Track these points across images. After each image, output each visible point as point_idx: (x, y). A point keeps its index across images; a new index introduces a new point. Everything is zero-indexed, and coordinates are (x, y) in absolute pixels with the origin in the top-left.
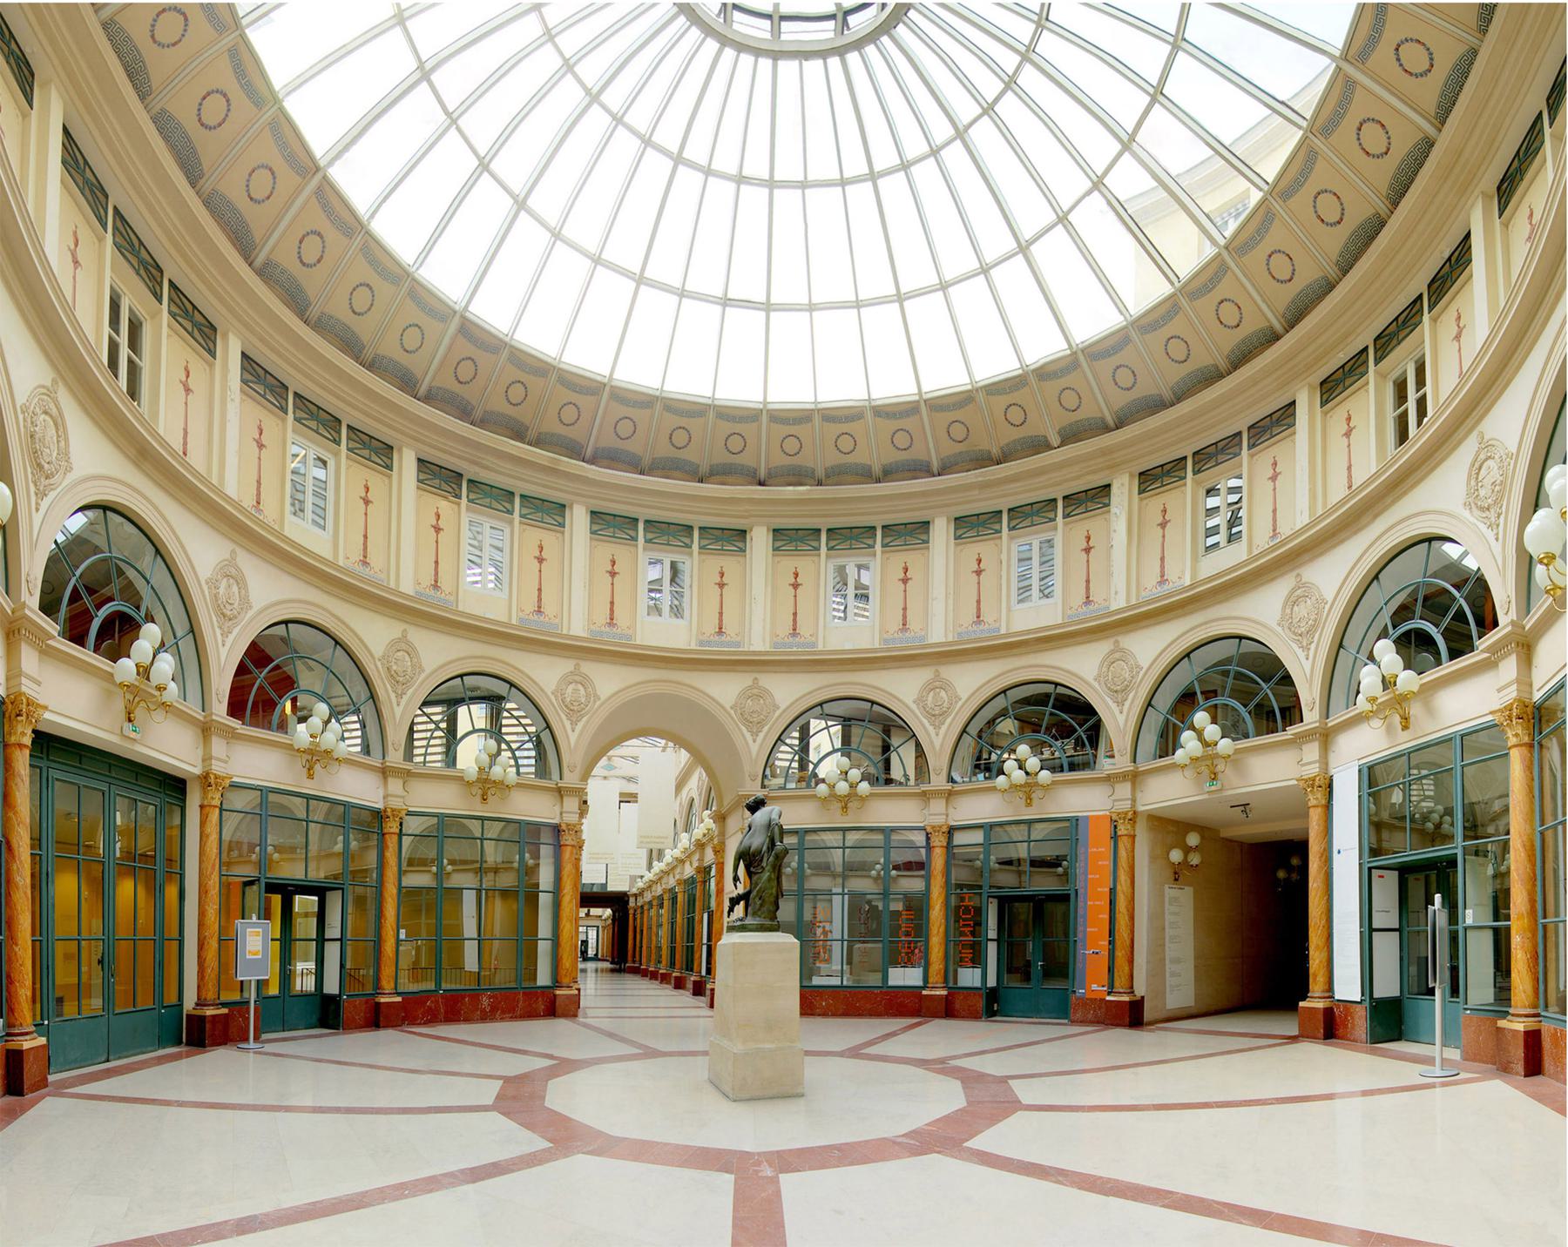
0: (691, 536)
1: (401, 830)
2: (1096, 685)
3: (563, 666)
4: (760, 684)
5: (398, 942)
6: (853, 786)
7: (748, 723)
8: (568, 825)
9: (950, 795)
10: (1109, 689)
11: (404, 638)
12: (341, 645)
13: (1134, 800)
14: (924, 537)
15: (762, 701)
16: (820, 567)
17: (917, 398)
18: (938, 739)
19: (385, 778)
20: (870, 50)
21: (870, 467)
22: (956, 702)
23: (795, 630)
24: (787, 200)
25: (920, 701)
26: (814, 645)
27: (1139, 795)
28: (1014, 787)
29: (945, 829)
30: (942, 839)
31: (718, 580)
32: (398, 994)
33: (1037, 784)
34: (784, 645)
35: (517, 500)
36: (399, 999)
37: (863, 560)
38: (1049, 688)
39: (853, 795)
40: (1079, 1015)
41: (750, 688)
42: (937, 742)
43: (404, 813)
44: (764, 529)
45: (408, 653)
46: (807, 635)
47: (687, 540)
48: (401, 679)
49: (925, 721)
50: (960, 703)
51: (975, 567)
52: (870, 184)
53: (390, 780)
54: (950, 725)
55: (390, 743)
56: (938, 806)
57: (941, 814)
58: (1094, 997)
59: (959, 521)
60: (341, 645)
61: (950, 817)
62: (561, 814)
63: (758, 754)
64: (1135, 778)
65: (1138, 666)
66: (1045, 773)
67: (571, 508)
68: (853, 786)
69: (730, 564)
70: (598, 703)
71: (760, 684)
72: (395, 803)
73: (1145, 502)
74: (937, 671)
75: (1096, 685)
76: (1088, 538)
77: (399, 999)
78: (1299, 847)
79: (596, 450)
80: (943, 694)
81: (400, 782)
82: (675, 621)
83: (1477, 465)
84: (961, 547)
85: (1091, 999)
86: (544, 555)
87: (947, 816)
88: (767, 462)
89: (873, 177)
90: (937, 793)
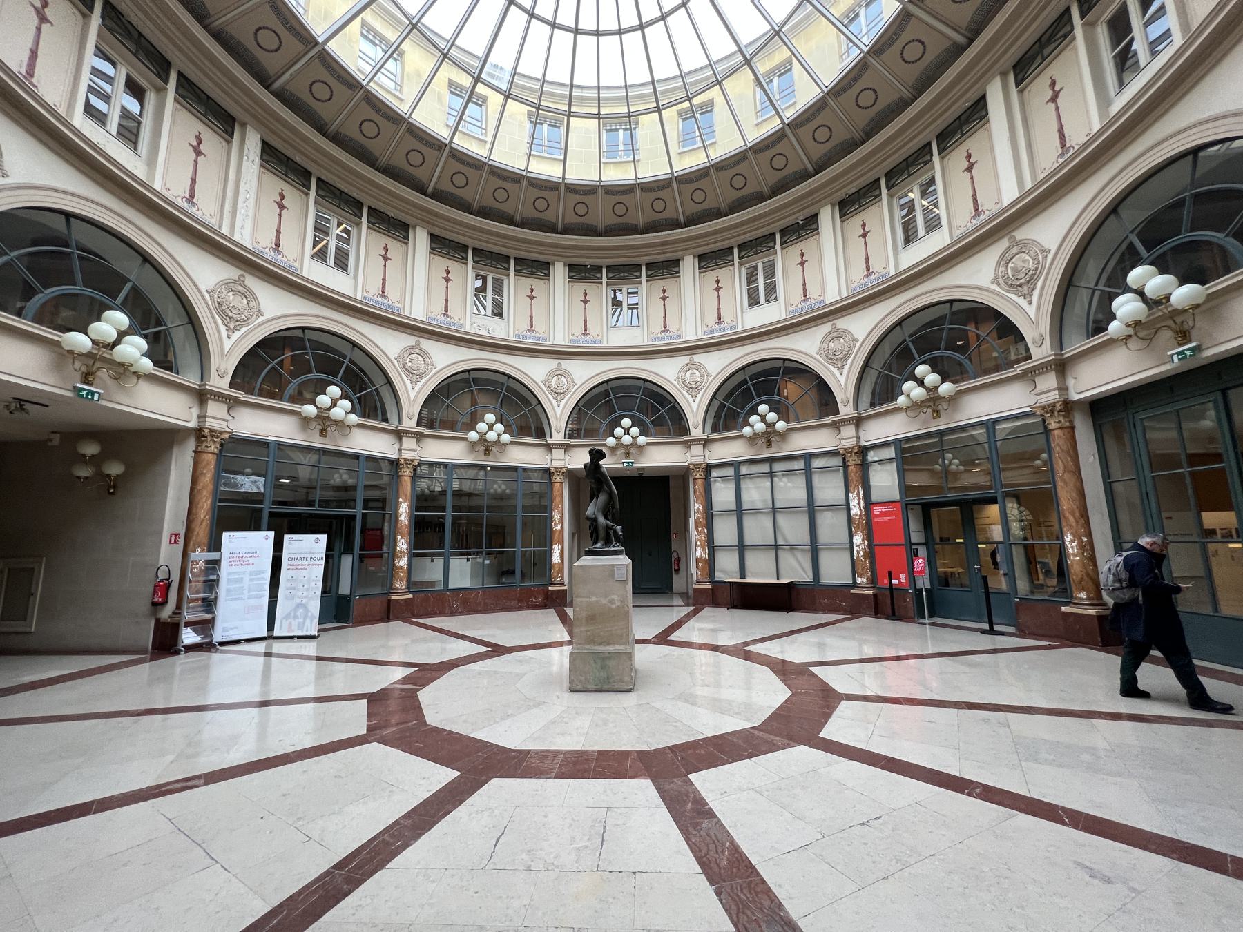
2: (995, 287)
3: (549, 364)
6: (634, 438)
8: (555, 468)
9: (706, 443)
10: (1011, 286)
11: (417, 345)
12: (358, 347)
13: (858, 438)
14: (676, 269)
15: (842, 340)
16: (601, 293)
18: (695, 408)
19: (400, 439)
21: (637, 225)
23: (585, 331)
24: (586, 42)
25: (547, 381)
26: (735, 327)
27: (861, 433)
29: (703, 466)
30: (702, 473)
31: (662, 295)
32: (410, 592)
33: (940, 398)
35: (470, 253)
38: (780, 363)
46: (595, 335)
47: (506, 265)
49: (550, 396)
50: (858, 345)
54: (568, 401)
55: (404, 414)
57: (853, 438)
59: (702, 258)
60: (358, 347)
61: (862, 439)
64: (1061, 366)
65: (708, 374)
67: (553, 264)
68: (634, 438)
69: (537, 284)
70: (710, 379)
71: (838, 327)
73: (703, 274)
75: (995, 287)
77: (411, 596)
79: (523, 219)
80: (697, 373)
83: (1008, 256)
88: (481, 198)
90: (696, 442)
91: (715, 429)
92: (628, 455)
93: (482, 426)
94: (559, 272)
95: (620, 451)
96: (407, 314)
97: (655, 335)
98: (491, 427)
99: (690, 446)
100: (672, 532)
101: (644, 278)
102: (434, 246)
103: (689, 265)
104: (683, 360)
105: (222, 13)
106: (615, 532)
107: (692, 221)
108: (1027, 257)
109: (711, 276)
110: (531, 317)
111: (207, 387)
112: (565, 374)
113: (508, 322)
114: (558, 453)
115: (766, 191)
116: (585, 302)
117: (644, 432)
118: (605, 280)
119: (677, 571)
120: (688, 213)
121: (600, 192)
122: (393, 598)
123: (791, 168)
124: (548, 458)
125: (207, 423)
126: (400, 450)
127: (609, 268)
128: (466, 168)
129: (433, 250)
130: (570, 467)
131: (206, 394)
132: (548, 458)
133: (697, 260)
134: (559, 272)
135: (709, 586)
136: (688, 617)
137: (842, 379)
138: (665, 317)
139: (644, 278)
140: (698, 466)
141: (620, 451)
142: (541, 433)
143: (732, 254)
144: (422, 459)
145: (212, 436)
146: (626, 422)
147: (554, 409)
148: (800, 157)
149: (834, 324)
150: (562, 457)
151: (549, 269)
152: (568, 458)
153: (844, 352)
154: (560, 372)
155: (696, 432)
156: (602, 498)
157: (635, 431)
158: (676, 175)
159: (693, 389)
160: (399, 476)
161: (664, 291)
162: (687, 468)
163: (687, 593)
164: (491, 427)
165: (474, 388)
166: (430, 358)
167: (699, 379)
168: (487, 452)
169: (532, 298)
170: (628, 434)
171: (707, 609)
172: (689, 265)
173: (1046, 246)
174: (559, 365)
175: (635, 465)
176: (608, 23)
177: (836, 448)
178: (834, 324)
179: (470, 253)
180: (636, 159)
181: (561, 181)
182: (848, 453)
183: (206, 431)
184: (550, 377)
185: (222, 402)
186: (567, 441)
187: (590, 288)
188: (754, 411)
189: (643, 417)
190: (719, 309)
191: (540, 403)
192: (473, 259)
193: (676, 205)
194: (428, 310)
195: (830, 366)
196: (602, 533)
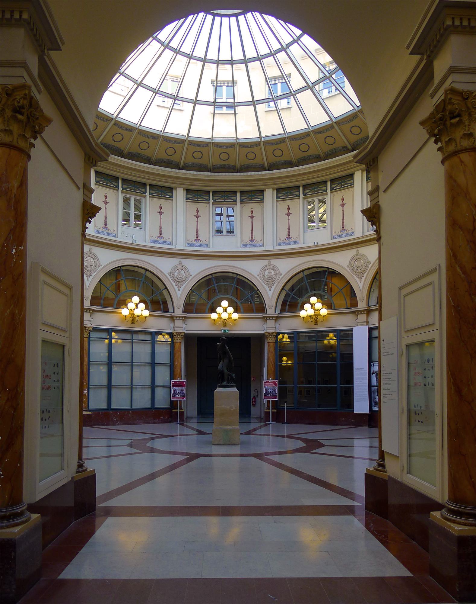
1: (89, 336)
2: (258, 278)
3: (173, 262)
4: (360, 252)
5: (253, 401)
8: (177, 333)
9: (277, 319)
15: (362, 261)
19: (174, 321)
24: (168, 54)
25: (172, 274)
27: (370, 320)
29: (274, 334)
30: (273, 339)
35: (120, 182)
36: (90, 413)
37: (321, 198)
41: (356, 255)
43: (91, 329)
45: (93, 258)
46: (204, 240)
48: (89, 269)
49: (265, 285)
50: (371, 265)
56: (271, 323)
59: (278, 190)
62: (174, 327)
63: (272, 296)
69: (165, 203)
70: (281, 276)
71: (272, 263)
73: (279, 202)
75: (258, 278)
76: (343, 199)
77: (90, 413)
80: (183, 272)
87: (275, 328)
90: (270, 318)
94: (180, 194)
97: (245, 243)
98: (137, 305)
100: (251, 376)
101: (238, 201)
103: (269, 195)
104: (263, 263)
106: (232, 377)
107: (272, 167)
109: (284, 205)
110: (161, 227)
112: (184, 268)
113: (145, 231)
114: (178, 323)
115: (322, 155)
116: (197, 217)
118: (211, 201)
119: (254, 405)
120: (270, 162)
123: (337, 145)
124: (172, 325)
127: (214, 193)
132: (172, 325)
133: (275, 191)
134: (180, 194)
136: (261, 427)
137: (361, 285)
139: (238, 201)
140: (271, 334)
142: (167, 310)
146: (225, 303)
147: (176, 293)
148: (343, 140)
149: (358, 250)
153: (363, 269)
154: (180, 267)
155: (270, 311)
156: (226, 361)
157: (231, 310)
158: (263, 139)
159: (270, 283)
161: (252, 212)
162: (264, 334)
163: (260, 417)
164: (137, 305)
166: (98, 259)
167: (274, 276)
169: (161, 213)
170: (226, 311)
172: (269, 195)
173: (370, 260)
174: (180, 262)
175: (229, 332)
176: (225, 56)
180: (236, 112)
181: (186, 138)
184: (174, 271)
187: (201, 207)
189: (237, 301)
190: (289, 228)
191: (166, 288)
193: (262, 154)
195: (354, 276)
196: (226, 377)
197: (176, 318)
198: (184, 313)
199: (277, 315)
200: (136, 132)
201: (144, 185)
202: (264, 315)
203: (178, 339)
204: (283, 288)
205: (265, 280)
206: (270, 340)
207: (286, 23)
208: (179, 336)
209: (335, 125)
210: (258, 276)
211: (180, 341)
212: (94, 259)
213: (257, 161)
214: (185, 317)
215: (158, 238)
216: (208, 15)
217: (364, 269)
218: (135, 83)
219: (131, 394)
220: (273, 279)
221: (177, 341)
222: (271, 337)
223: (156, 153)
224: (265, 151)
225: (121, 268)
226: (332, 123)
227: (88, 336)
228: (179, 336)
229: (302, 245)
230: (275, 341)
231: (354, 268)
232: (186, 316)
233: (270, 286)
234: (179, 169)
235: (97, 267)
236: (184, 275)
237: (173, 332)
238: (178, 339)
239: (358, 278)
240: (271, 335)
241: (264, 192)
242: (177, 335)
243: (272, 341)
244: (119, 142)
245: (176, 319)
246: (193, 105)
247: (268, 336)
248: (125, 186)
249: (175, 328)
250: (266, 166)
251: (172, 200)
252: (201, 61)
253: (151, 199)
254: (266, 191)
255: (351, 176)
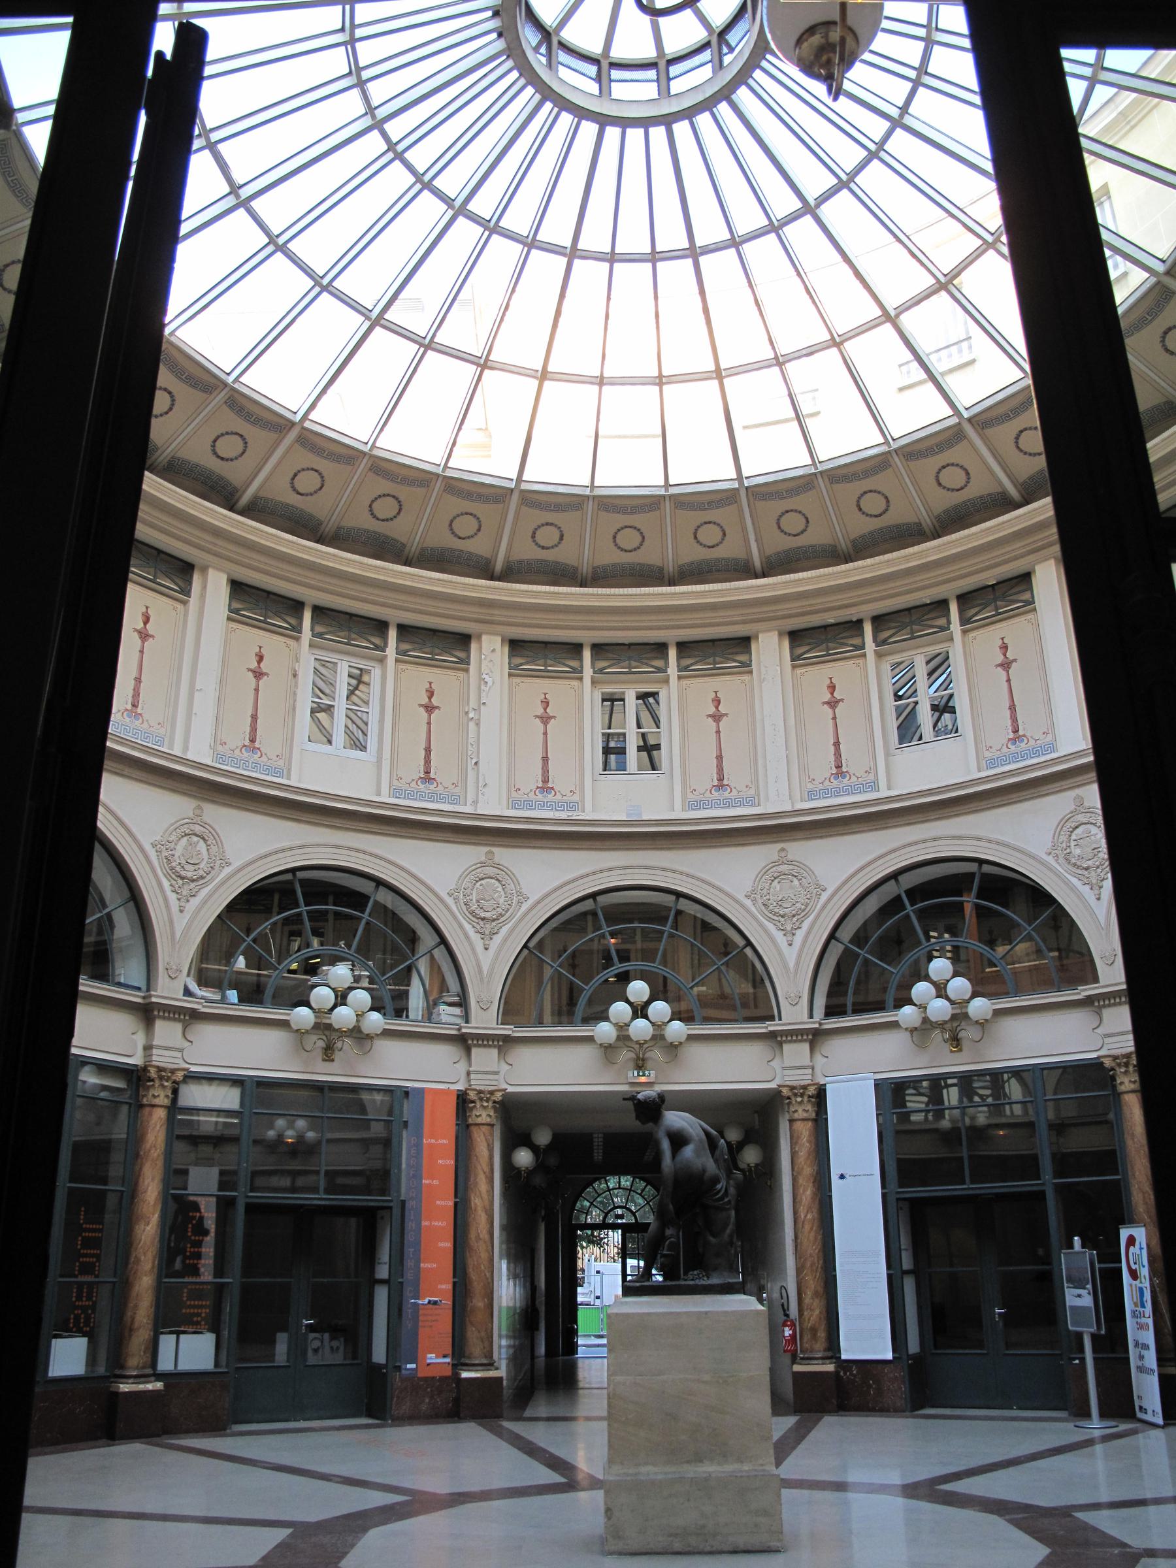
0: (665, 657)
1: (175, 1100)
6: (658, 1027)
7: (777, 917)
9: (815, 1037)
10: (472, 913)
17: (955, 420)
20: (704, 120)
22: (520, 903)
23: (1016, 731)
28: (927, 1025)
29: (812, 1091)
30: (809, 1107)
32: (159, 1376)
34: (1003, 761)
35: (307, 616)
36: (159, 1385)
38: (972, 867)
39: (960, 1016)
40: (406, 1408)
42: (791, 955)
44: (773, 637)
46: (861, 773)
50: (825, 896)
51: (1000, 659)
52: (689, 262)
53: (160, 1026)
56: (797, 1052)
58: (430, 1374)
59: (796, 636)
62: (468, 1074)
65: (520, 894)
66: (677, 1025)
69: (444, 680)
72: (160, 1058)
74: (491, 852)
77: (159, 1385)
78: (1113, 1152)
81: (178, 1027)
82: (650, 777)
84: (802, 670)
85: (426, 1379)
86: (435, 701)
87: (813, 1068)
89: (694, 252)
90: (795, 1035)
91: (832, 1011)
92: (640, 1065)
93: (322, 995)
95: (625, 1055)
96: (177, 751)
98: (341, 998)
99: (781, 1044)
102: (236, 605)
105: (170, 441)
108: (500, 889)
111: (154, 1000)
114: (484, 1058)
117: (676, 1016)
121: (590, 506)
122: (465, 1375)
123: (975, 490)
125: (154, 1058)
126: (148, 1048)
128: (326, 462)
129: (234, 616)
130: (510, 1089)
131: (153, 1011)
133: (786, 643)
135: (830, 1367)
138: (720, 758)
139: (673, 670)
141: (625, 1055)
143: (861, 634)
144: (193, 1068)
145: (161, 1078)
150: (807, 1062)
151: (468, 650)
152: (505, 1067)
160: (142, 1106)
165: (303, 909)
168: (329, 1052)
171: (828, 1420)
177: (1094, 1055)
178: (1078, 797)
179: (307, 616)
182: (1119, 1065)
183: (153, 1071)
185: (174, 1020)
186: (508, 1030)
188: (920, 975)
192: (312, 630)
194: (217, 741)
197: (475, 1042)
198: (502, 1024)
199: (817, 1026)
200: (364, 464)
201: (381, 626)
202: (772, 1026)
203: (483, 1115)
204: (832, 936)
205: (1075, 865)
206: (796, 1111)
207: (284, 1533)
208: (485, 1104)
209: (968, 428)
210: (748, 897)
211: (488, 1120)
212: (209, 843)
213: (729, 551)
214: (507, 1039)
215: (419, 782)
216: (584, 123)
217: (803, 907)
218: (368, 318)
219: (420, 916)
220: (499, 910)
221: (479, 1120)
222: (799, 1099)
223: (419, 534)
224: (461, 1179)
225: (294, 875)
226: (959, 424)
227: (167, 1102)
228: (485, 1104)
229: (884, 793)
230: (814, 1115)
231: (1070, 853)
232: (508, 1036)
233: (789, 928)
234: (492, 578)
235: (217, 868)
236: (504, 895)
237: (467, 1089)
238: (484, 1114)
239: (1087, 887)
240: (802, 1095)
241: (753, 646)
242: (481, 1099)
243: (805, 1115)
244: (311, 494)
245: (476, 1046)
246: (564, 260)
247: (789, 1098)
248: (319, 629)
249: (472, 1076)
250: (757, 563)
251: (467, 670)
252: (564, 255)
253: (402, 666)
254: (757, 637)
255: (1025, 578)
